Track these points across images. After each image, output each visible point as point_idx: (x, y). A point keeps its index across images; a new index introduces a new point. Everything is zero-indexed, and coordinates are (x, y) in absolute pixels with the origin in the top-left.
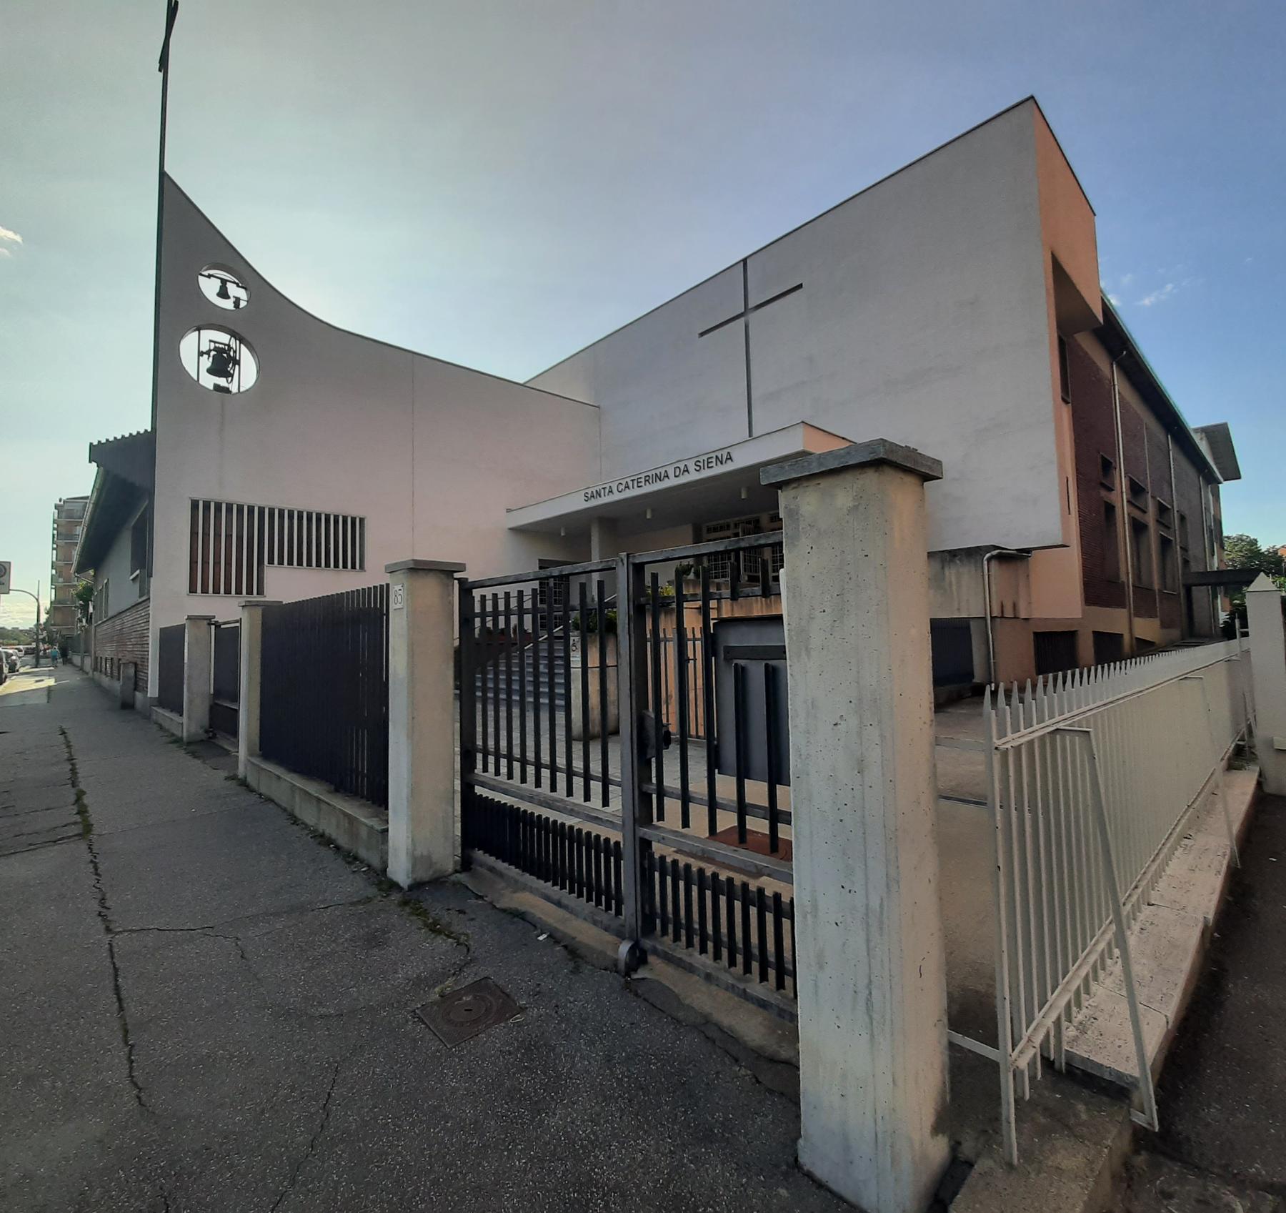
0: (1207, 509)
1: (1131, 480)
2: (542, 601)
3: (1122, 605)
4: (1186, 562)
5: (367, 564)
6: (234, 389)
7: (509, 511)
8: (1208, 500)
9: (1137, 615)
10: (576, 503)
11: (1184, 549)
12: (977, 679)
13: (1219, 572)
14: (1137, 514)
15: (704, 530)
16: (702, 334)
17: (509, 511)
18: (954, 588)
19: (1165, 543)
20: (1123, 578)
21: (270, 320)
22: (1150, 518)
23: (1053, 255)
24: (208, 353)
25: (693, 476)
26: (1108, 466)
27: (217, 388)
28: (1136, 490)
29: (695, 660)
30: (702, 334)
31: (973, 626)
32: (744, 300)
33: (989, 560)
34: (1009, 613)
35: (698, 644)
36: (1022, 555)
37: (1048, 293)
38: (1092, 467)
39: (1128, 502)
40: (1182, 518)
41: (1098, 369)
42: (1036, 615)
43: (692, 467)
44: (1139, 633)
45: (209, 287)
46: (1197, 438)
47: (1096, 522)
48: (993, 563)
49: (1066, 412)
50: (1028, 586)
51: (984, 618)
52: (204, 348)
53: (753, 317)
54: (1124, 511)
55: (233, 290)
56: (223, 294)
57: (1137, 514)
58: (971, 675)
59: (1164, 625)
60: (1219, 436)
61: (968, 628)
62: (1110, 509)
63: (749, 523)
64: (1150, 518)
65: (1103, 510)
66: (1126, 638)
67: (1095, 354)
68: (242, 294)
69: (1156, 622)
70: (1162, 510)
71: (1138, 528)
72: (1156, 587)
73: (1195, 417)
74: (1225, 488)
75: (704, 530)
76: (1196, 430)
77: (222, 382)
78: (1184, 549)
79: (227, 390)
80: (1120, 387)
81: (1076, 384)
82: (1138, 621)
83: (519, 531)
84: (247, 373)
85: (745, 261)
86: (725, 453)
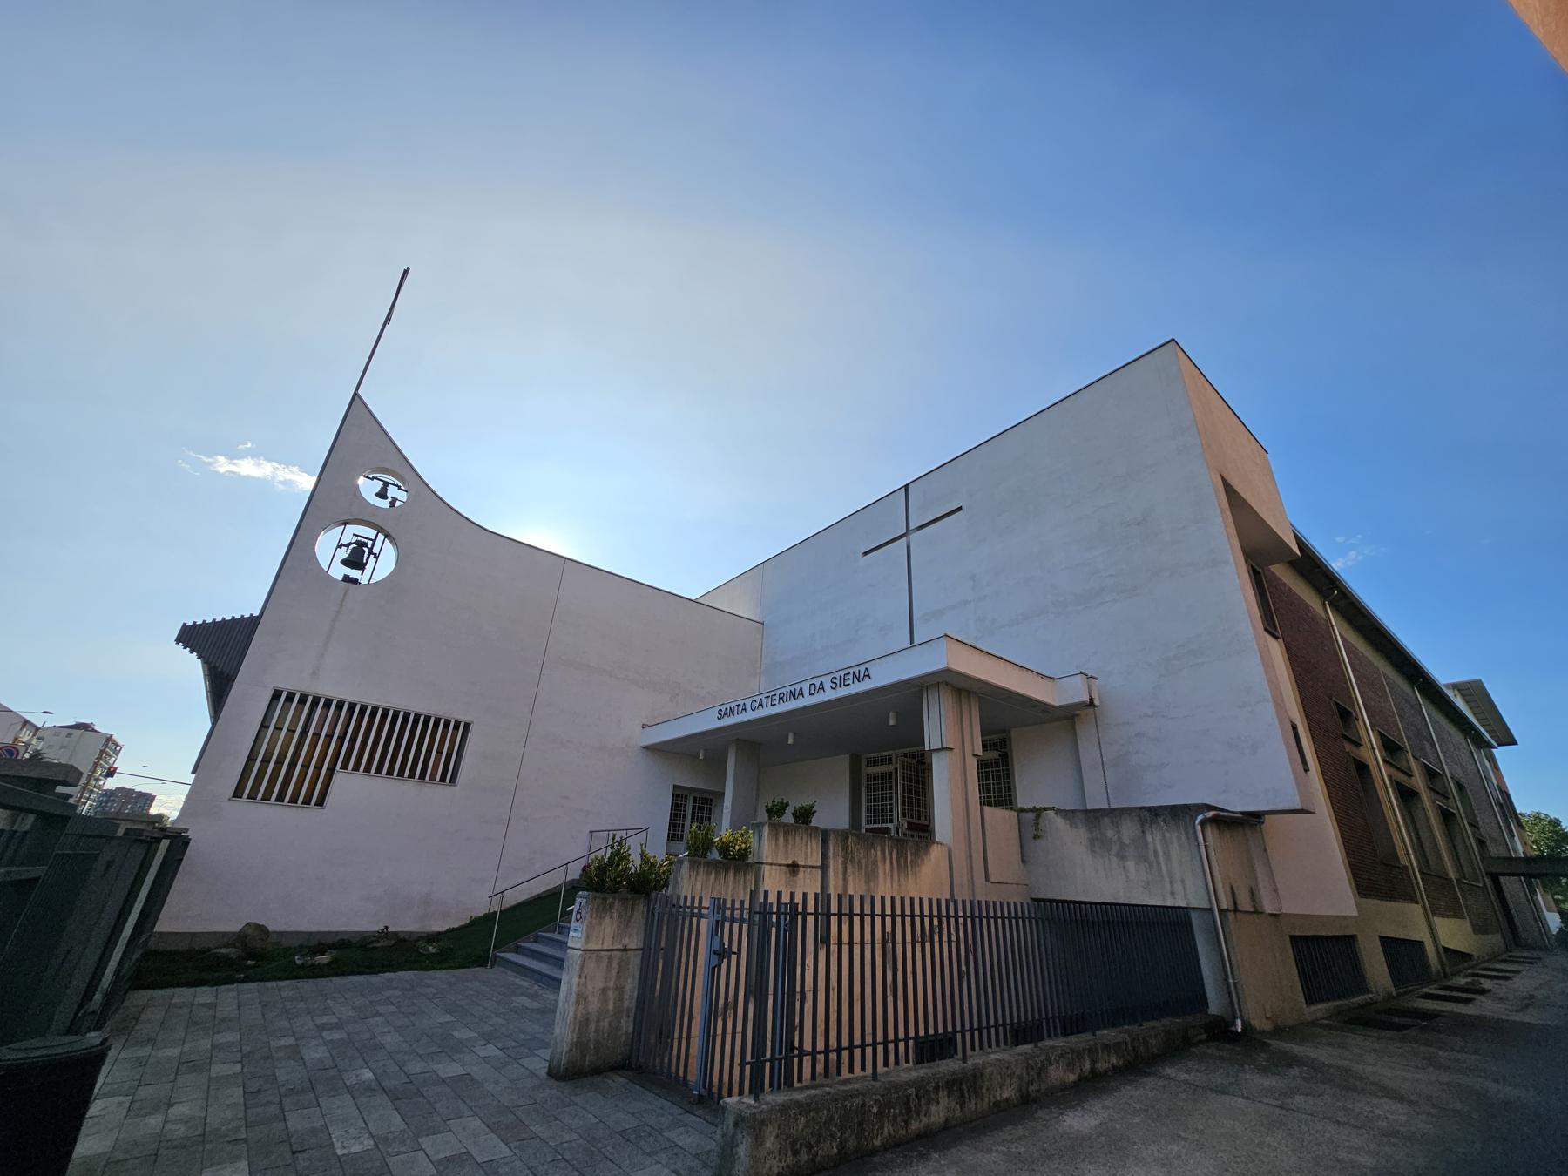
0: (1489, 779)
1: (1381, 735)
2: (128, 832)
3: (1411, 898)
4: (1481, 843)
5: (461, 778)
6: (364, 581)
7: (645, 726)
8: (1485, 768)
9: (1434, 914)
10: (709, 722)
11: (1474, 825)
12: (1214, 1009)
13: (1528, 860)
14: (1401, 777)
15: (864, 763)
16: (866, 554)
17: (645, 726)
18: (1161, 858)
19: (1447, 817)
20: (1404, 861)
21: (426, 520)
22: (1419, 782)
23: (1223, 479)
24: (347, 546)
25: (829, 695)
26: (1346, 716)
27: (347, 579)
28: (1391, 748)
29: (739, 953)
30: (866, 554)
31: (1194, 916)
32: (904, 522)
33: (1203, 823)
34: (1245, 903)
35: (810, 919)
36: (1253, 820)
37: (1222, 511)
38: (1327, 717)
39: (1385, 761)
40: (1460, 787)
41: (1308, 606)
42: (1289, 908)
43: (827, 685)
44: (1447, 941)
45: (367, 488)
46: (1450, 694)
47: (1349, 787)
48: (1209, 830)
49: (1276, 648)
50: (1268, 863)
51: (1210, 910)
52: (344, 541)
53: (914, 537)
54: (1381, 771)
55: (392, 492)
56: (382, 494)
57: (1401, 777)
58: (1202, 1000)
59: (1479, 929)
60: (1475, 692)
61: (1189, 924)
62: (1362, 768)
63: (913, 757)
64: (1419, 782)
65: (1353, 768)
66: (1430, 948)
67: (1295, 589)
68: (402, 496)
69: (1465, 925)
70: (1432, 775)
71: (1407, 795)
72: (1452, 874)
73: (1444, 673)
74: (1500, 753)
75: (864, 763)
76: (1447, 686)
77: (354, 573)
78: (1474, 825)
79: (355, 581)
80: (1339, 628)
81: (1276, 613)
82: (1438, 922)
83: (654, 750)
84: (384, 563)
85: (906, 487)
86: (862, 669)
